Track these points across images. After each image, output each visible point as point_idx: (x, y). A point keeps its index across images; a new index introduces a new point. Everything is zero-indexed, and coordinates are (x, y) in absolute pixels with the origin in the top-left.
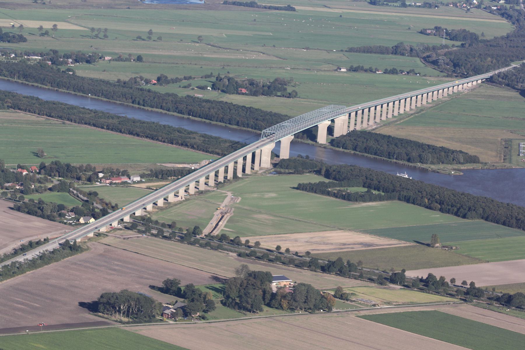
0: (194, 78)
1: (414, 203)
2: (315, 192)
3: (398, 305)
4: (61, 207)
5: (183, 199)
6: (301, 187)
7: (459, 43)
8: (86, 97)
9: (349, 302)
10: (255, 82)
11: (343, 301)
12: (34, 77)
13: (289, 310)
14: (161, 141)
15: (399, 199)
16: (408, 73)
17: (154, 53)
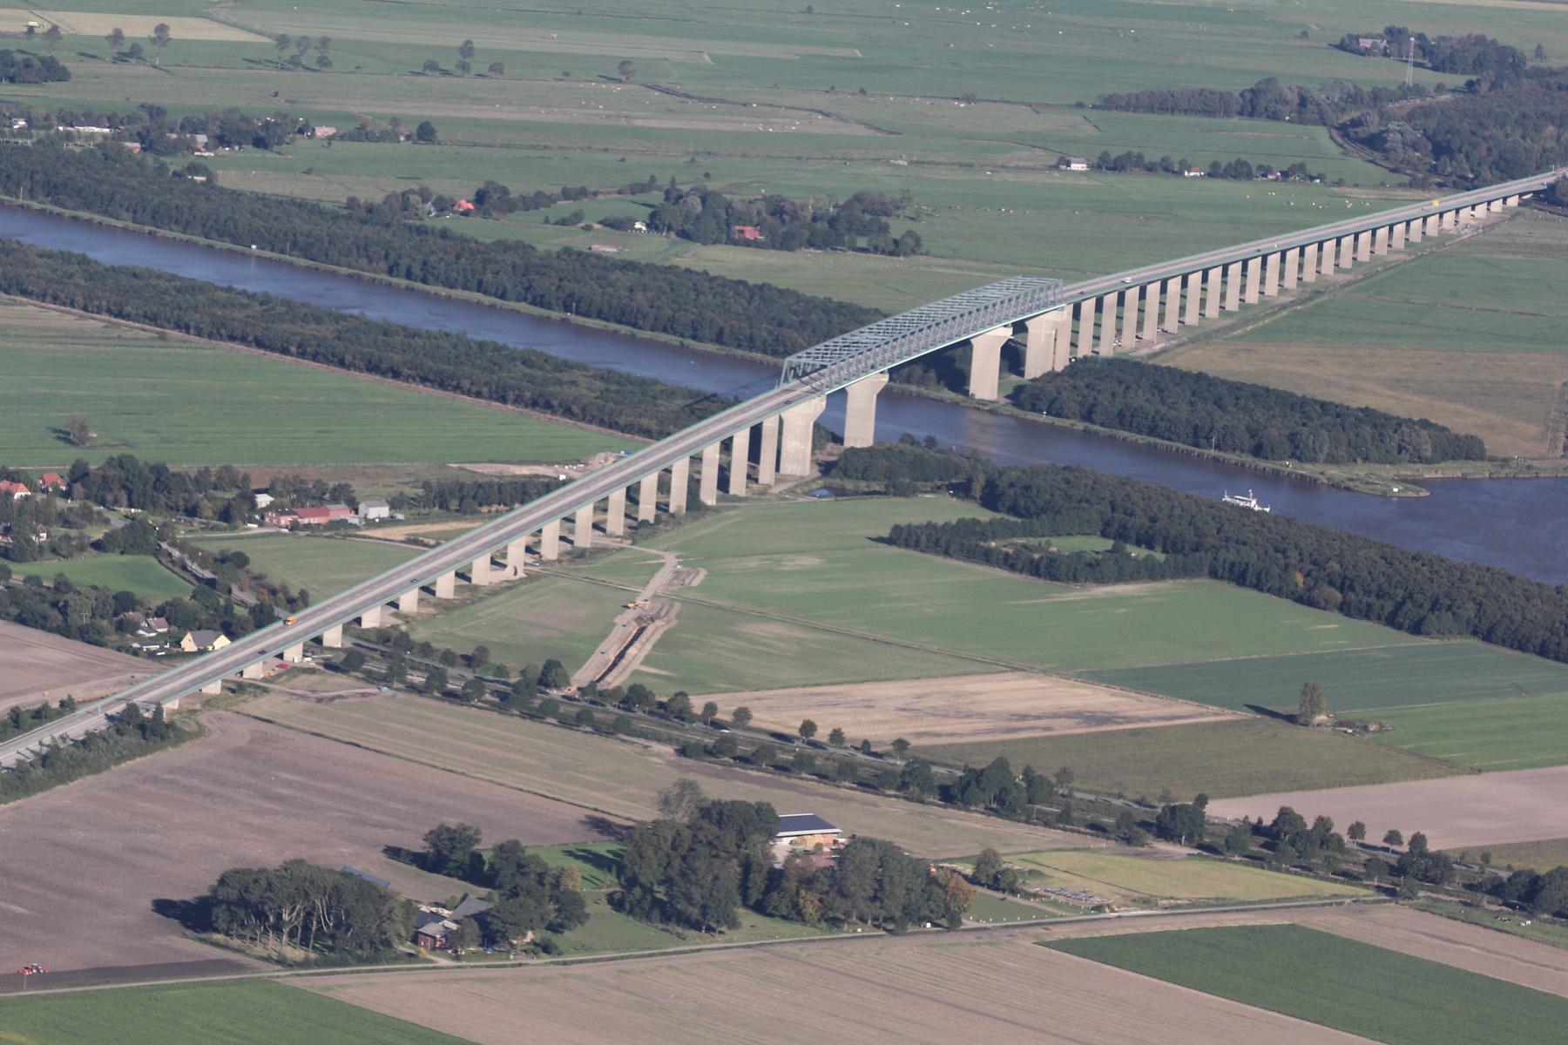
0: (595, 194)
1: (1258, 587)
2: (947, 553)
3: (1175, 909)
4: (125, 602)
5: (521, 574)
6: (901, 537)
7: (1459, 80)
8: (243, 254)
9: (1018, 899)
10: (788, 207)
11: (999, 895)
12: (79, 191)
13: (824, 925)
14: (469, 393)
15: (1214, 574)
16: (1285, 174)
17: (474, 115)
